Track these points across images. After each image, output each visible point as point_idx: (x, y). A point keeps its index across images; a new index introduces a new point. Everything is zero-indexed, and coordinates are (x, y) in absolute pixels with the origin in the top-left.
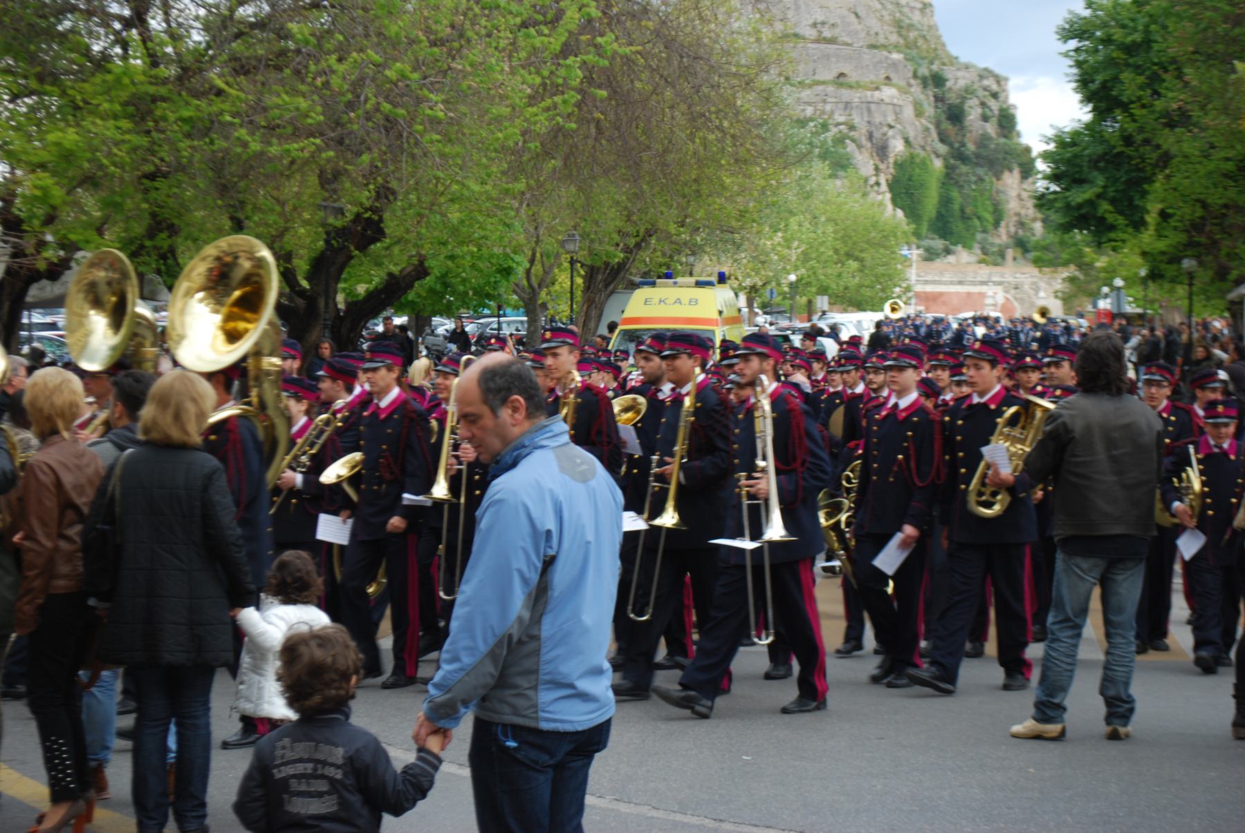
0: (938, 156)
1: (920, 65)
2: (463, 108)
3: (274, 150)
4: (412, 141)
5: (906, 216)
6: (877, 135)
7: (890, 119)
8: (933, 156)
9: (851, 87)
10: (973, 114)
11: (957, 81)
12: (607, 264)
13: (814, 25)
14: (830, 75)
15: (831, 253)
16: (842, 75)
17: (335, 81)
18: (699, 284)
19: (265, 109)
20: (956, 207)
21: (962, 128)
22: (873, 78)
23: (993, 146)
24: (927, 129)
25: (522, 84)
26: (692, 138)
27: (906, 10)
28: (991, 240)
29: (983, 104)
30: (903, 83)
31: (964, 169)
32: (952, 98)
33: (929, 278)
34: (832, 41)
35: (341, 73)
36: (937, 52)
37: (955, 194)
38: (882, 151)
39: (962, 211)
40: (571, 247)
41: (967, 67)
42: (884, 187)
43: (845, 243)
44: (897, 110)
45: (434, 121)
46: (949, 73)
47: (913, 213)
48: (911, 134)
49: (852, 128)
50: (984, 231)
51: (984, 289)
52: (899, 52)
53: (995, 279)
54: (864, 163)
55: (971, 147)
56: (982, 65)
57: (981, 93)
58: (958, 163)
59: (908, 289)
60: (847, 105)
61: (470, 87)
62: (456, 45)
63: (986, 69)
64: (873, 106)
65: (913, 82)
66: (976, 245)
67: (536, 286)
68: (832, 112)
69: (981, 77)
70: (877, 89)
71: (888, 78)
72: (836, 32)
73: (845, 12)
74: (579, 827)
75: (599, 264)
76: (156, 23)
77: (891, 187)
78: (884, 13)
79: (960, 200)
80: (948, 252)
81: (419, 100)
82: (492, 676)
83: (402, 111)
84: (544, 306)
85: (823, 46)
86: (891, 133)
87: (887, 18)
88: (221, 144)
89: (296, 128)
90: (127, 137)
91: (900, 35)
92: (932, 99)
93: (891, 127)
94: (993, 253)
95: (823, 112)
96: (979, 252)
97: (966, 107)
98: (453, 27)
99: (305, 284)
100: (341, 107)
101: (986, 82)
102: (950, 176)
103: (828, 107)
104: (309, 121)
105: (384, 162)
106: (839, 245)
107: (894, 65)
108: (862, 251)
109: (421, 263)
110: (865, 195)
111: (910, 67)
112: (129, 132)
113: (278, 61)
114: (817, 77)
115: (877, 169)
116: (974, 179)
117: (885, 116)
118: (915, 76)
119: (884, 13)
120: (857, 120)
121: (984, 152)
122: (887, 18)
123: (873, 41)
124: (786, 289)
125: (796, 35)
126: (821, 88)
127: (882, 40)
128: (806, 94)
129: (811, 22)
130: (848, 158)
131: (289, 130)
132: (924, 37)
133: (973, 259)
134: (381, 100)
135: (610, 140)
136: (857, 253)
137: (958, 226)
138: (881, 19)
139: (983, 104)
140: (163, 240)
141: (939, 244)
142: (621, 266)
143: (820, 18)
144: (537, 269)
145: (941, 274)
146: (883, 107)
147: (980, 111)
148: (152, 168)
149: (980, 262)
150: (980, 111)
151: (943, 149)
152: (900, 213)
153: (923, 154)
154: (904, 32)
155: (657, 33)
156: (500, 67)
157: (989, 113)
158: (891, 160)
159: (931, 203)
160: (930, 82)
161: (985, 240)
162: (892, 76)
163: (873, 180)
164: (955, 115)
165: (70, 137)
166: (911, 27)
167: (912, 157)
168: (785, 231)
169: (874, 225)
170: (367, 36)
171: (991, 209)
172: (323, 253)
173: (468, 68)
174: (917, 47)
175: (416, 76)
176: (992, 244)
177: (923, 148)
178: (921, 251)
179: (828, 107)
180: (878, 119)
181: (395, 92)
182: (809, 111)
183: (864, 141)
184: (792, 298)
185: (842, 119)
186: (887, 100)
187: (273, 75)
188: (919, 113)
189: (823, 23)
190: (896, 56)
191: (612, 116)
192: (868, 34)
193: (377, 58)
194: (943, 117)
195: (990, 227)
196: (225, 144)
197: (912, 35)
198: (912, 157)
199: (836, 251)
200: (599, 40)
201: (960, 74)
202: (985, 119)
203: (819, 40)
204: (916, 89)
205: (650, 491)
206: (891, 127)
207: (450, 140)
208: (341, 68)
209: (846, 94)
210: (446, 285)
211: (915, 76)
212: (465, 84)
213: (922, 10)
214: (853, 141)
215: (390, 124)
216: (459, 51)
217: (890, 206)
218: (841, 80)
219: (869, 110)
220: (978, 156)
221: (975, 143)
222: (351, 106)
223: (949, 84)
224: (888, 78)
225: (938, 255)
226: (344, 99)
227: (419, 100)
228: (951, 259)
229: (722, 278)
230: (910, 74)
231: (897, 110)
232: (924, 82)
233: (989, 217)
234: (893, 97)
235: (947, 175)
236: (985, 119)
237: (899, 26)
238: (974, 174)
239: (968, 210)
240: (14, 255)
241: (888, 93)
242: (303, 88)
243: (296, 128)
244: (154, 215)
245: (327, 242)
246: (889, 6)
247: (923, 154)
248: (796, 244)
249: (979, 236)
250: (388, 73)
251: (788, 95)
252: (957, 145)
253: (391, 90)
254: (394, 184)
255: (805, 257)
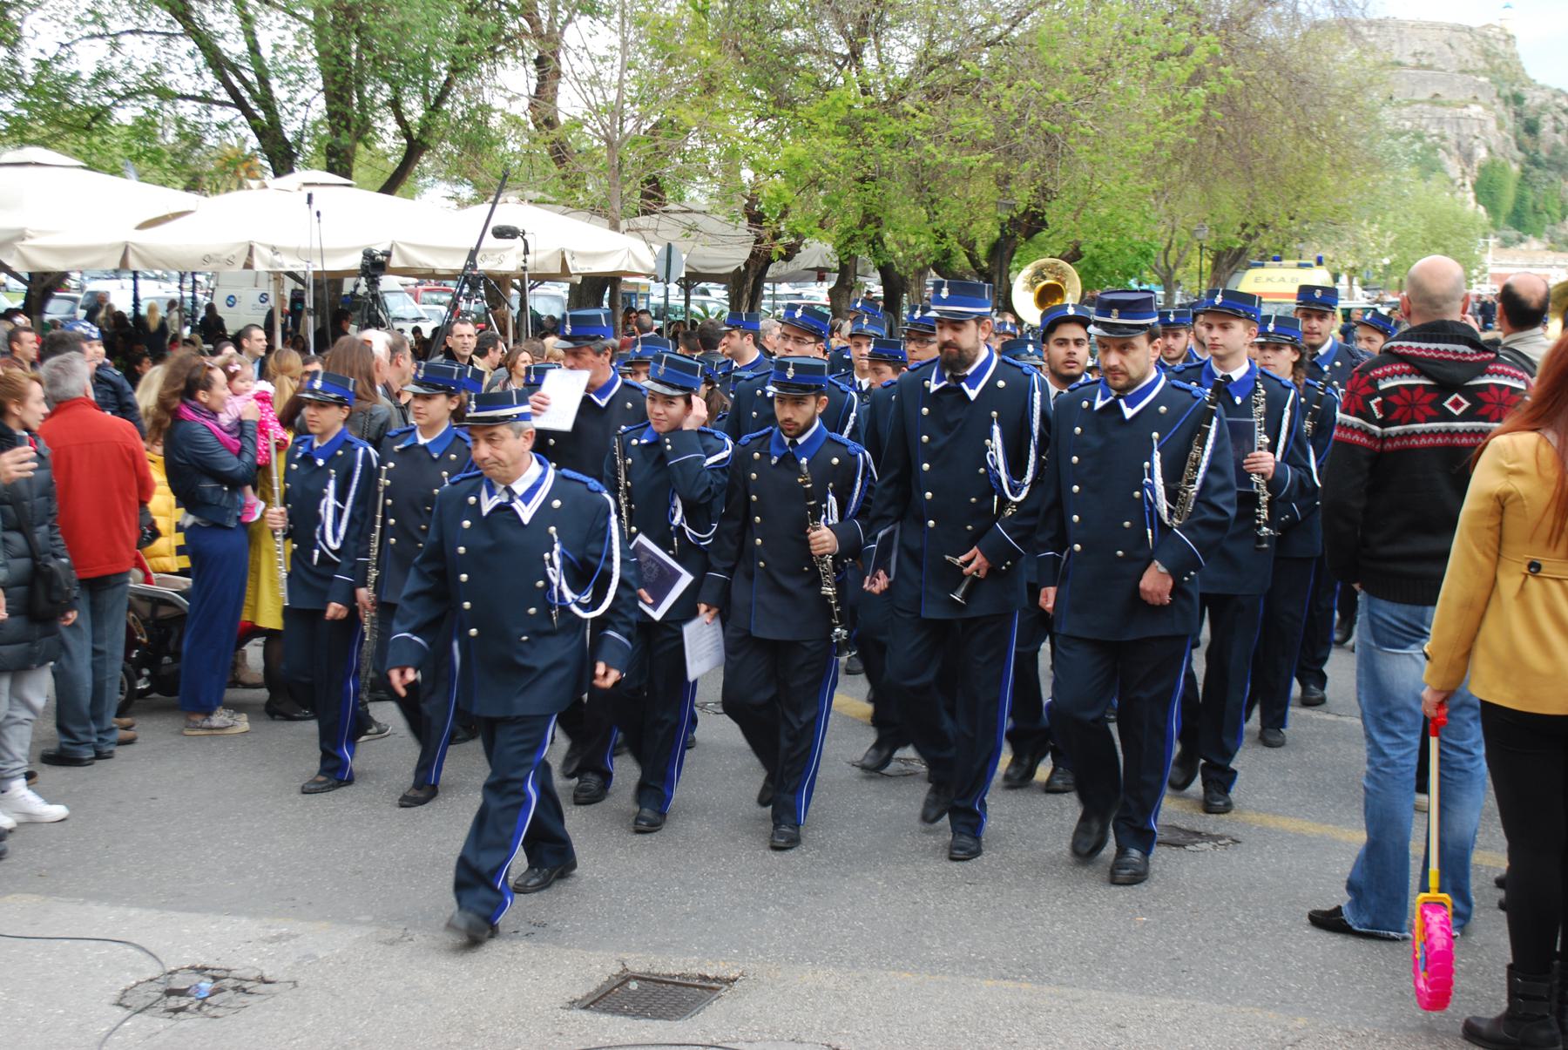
0: (1515, 161)
1: (1502, 86)
2: (1107, 124)
3: (955, 161)
4: (1065, 150)
5: (1487, 211)
6: (1464, 144)
7: (1476, 132)
8: (1511, 162)
9: (1443, 105)
10: (1546, 127)
11: (1533, 99)
12: (1230, 249)
13: (1415, 54)
14: (1425, 96)
15: (1419, 241)
16: (1437, 95)
17: (1005, 105)
18: (1300, 266)
19: (949, 127)
20: (1529, 203)
21: (1536, 138)
22: (1462, 97)
23: (1562, 154)
24: (1507, 140)
25: (1155, 105)
26: (1297, 148)
27: (1493, 41)
28: (1557, 230)
29: (1555, 119)
30: (1488, 102)
31: (1537, 172)
32: (1530, 115)
33: (1503, 262)
34: (1429, 67)
35: (1009, 100)
36: (1518, 76)
37: (1529, 193)
38: (1468, 157)
39: (1535, 207)
40: (1200, 235)
41: (1543, 88)
42: (1469, 187)
43: (1432, 233)
44: (1482, 124)
45: (1084, 136)
46: (1528, 93)
47: (1492, 209)
48: (1493, 143)
49: (1443, 138)
50: (1553, 224)
51: (1548, 271)
52: (1486, 76)
53: (1559, 263)
54: (1453, 167)
55: (1544, 154)
56: (1555, 86)
57: (1554, 109)
58: (1533, 167)
59: (1484, 271)
60: (1440, 120)
61: (1113, 108)
62: (1103, 73)
63: (1559, 90)
64: (1462, 121)
65: (1496, 100)
66: (1546, 235)
67: (1171, 265)
68: (1427, 126)
69: (1555, 96)
70: (1466, 106)
71: (1475, 98)
72: (1433, 59)
73: (1441, 44)
74: (7, 892)
75: (1223, 249)
76: (870, 60)
77: (1475, 187)
78: (1474, 44)
79: (1533, 198)
80: (1521, 240)
81: (1072, 118)
82: (1489, 528)
83: (1058, 127)
84: (1178, 283)
85: (1420, 72)
86: (1476, 142)
87: (1476, 48)
88: (914, 154)
89: (975, 143)
90: (842, 151)
91: (1487, 62)
92: (1512, 115)
93: (1476, 138)
94: (1559, 242)
95: (1420, 126)
96: (1547, 240)
97: (1541, 121)
98: (1102, 59)
99: (985, 265)
100: (1009, 124)
101: (1558, 101)
102: (1525, 178)
103: (1424, 122)
104: (983, 137)
105: (1043, 168)
106: (1426, 234)
107: (1481, 87)
108: (1446, 239)
109: (1077, 248)
110: (1453, 193)
111: (1494, 88)
112: (845, 146)
113: (962, 87)
114: (1416, 98)
115: (1463, 172)
116: (1545, 180)
117: (1472, 129)
118: (1498, 96)
119: (1474, 44)
120: (1448, 132)
121: (1554, 158)
122: (1476, 48)
123: (1463, 67)
124: (1380, 270)
125: (1399, 64)
126: (1419, 106)
127: (1471, 66)
128: (1405, 111)
129: (1411, 52)
130: (1440, 163)
131: (969, 143)
132: (1507, 64)
133: (1542, 246)
134: (1041, 118)
135: (1230, 149)
136: (1441, 241)
137: (1530, 219)
138: (1471, 49)
139: (1555, 119)
140: (870, 229)
141: (1514, 234)
142: (1242, 251)
143: (1419, 48)
144: (1173, 253)
145: (1514, 258)
146: (1470, 121)
147: (1552, 124)
148: (861, 175)
149: (1549, 249)
150: (1552, 124)
151: (1520, 155)
152: (1481, 209)
153: (1502, 160)
154: (1490, 59)
155: (1270, 61)
156: (1138, 91)
157: (1560, 126)
158: (1476, 165)
159: (1508, 201)
160: (1511, 101)
161: (1553, 231)
162: (1478, 95)
163: (1460, 181)
164: (1531, 128)
165: (800, 151)
166: (1496, 55)
167: (1494, 162)
168: (1381, 223)
169: (1456, 217)
170: (1032, 67)
171: (1559, 205)
172: (998, 240)
173: (1112, 93)
174: (1501, 72)
175: (1069, 99)
176: (1558, 234)
177: (1503, 155)
178: (1497, 240)
179: (1424, 122)
180: (1465, 131)
181: (1053, 111)
182: (1408, 124)
183: (1453, 150)
184: (1386, 278)
185: (1435, 132)
186: (1474, 116)
187: (957, 99)
188: (1501, 127)
189: (1422, 53)
190: (1482, 79)
191: (1231, 130)
192: (1460, 61)
193: (1038, 85)
194: (1521, 130)
195: (1558, 220)
196: (918, 155)
197: (1497, 61)
198: (1494, 162)
199: (1424, 239)
200: (1222, 69)
201: (1537, 94)
202: (1557, 131)
203: (1419, 67)
204: (1499, 107)
205: (381, 489)
206: (1476, 138)
207: (1097, 150)
208: (1008, 93)
209: (1439, 111)
210: (1097, 266)
211: (1498, 96)
212: (1109, 105)
213: (1506, 41)
214: (1444, 149)
215: (1049, 137)
216: (1105, 79)
217: (1473, 203)
218: (1436, 99)
219: (1458, 125)
220: (1549, 161)
221: (1548, 151)
222: (1017, 123)
223: (1526, 102)
224: (1475, 98)
225: (1512, 243)
226: (1012, 118)
227: (1072, 118)
228: (1523, 246)
229: (1320, 261)
230: (1494, 94)
231: (1482, 124)
232: (1506, 101)
233: (1558, 213)
234: (1478, 113)
235: (1523, 178)
236: (1557, 131)
237: (1486, 54)
238: (1546, 176)
239: (1540, 206)
240: (757, 242)
241: (1475, 110)
242: (978, 110)
243: (975, 143)
244: (865, 210)
245: (1002, 231)
246: (1478, 38)
247: (1502, 160)
248: (1389, 233)
249: (1548, 228)
250: (1047, 95)
251: (1387, 115)
252: (1531, 153)
253: (1049, 109)
254: (1050, 186)
255: (1397, 245)
